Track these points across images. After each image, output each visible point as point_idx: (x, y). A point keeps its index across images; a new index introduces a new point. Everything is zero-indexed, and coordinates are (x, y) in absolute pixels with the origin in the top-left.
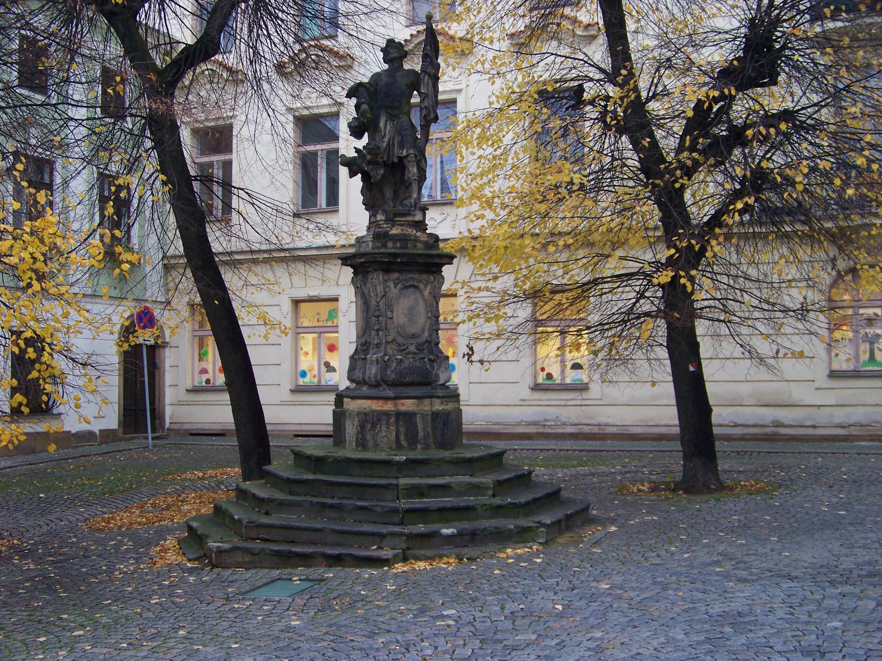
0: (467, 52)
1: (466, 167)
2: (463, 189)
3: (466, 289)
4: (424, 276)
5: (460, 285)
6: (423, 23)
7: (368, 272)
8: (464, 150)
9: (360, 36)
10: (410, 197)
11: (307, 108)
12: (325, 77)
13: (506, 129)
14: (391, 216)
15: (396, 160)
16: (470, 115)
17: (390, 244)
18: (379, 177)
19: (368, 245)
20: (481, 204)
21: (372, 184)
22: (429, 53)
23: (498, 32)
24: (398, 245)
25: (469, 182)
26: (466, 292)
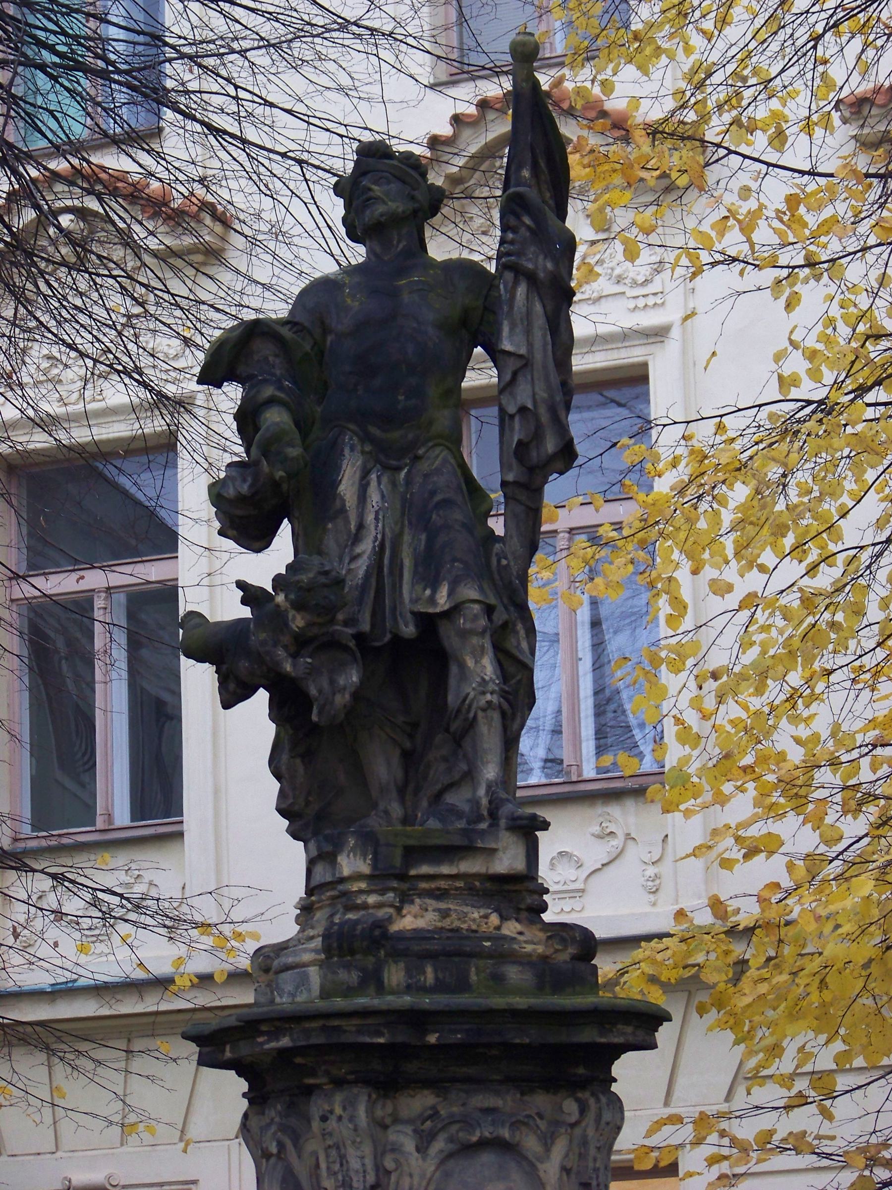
0: (683, 181)
1: (696, 645)
2: (687, 736)
3: (713, 1144)
4: (541, 1101)
5: (686, 1133)
6: (496, 72)
7: (309, 1091)
8: (683, 575)
9: (251, 134)
10: (470, 776)
11: (46, 423)
12: (116, 300)
13: (849, 485)
14: (398, 861)
15: (409, 630)
16: (704, 431)
17: (395, 975)
18: (341, 700)
19: (304, 981)
20: (764, 795)
21: (315, 729)
22: (531, 193)
23: (804, 98)
24: (429, 975)
25: (710, 703)
26: (713, 1161)
